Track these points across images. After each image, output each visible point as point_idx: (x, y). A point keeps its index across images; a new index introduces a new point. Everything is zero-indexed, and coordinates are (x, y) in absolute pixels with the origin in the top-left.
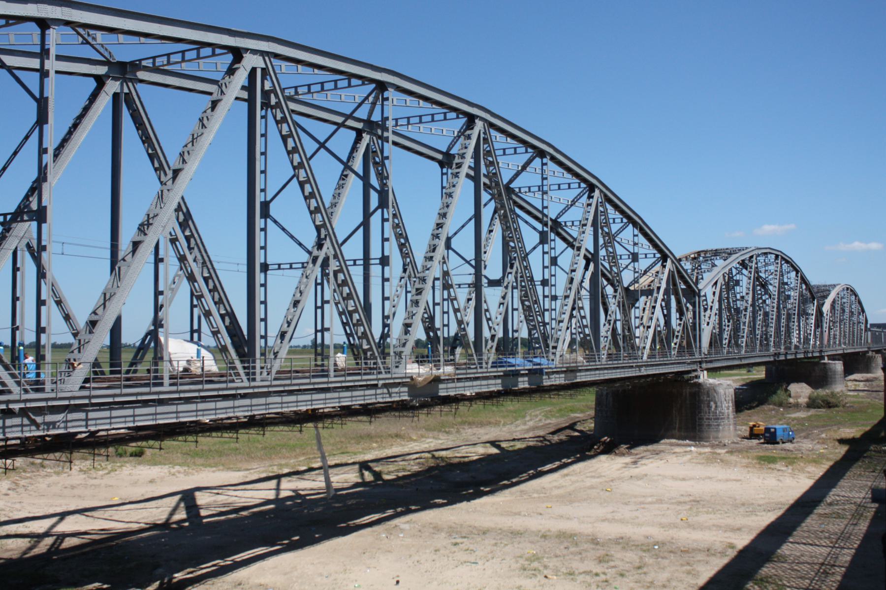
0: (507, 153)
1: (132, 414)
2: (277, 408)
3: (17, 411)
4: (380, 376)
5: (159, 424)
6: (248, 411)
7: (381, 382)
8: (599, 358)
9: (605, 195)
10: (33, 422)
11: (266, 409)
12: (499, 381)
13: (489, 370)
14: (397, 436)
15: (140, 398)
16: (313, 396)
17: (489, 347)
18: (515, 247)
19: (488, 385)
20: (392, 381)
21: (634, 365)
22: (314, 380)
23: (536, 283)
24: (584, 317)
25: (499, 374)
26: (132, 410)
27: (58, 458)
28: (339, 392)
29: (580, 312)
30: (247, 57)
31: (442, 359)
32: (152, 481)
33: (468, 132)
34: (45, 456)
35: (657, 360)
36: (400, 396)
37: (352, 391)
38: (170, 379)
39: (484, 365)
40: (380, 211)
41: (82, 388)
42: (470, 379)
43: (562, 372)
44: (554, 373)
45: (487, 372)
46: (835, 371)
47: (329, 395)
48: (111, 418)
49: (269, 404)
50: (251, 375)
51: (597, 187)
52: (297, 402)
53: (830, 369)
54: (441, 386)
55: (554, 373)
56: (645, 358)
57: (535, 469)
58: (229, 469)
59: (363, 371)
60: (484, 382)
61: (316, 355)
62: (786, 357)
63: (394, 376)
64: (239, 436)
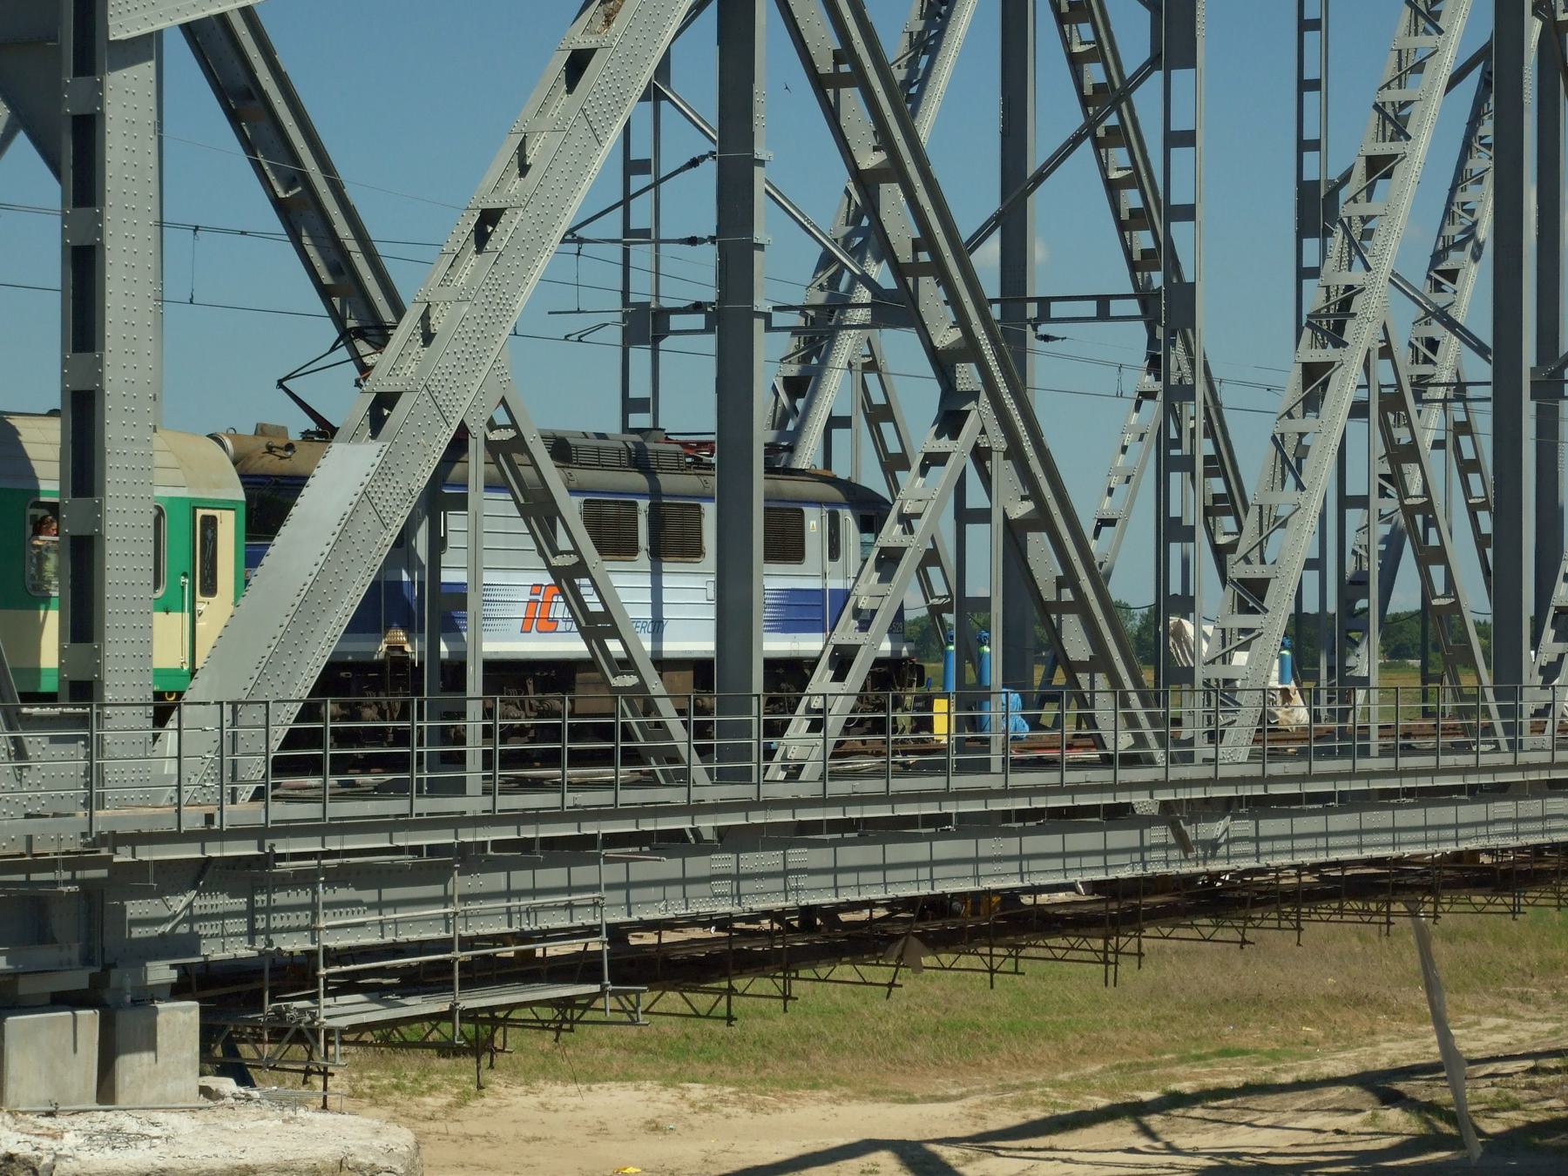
2: (1384, 845)
3: (708, 835)
4: (1363, 764)
5: (1117, 880)
6: (1316, 849)
11: (1394, 845)
14: (1358, 1001)
16: (1400, 814)
19: (785, 873)
20: (883, 811)
23: (1134, 307)
27: (822, 977)
28: (834, 844)
32: (654, 1127)
34: (823, 971)
35: (473, 804)
36: (977, 877)
37: (883, 841)
38: (987, 740)
40: (1157, 77)
42: (1477, 793)
48: (1257, 839)
49: (1493, 823)
52: (1361, 832)
58: (876, 1095)
60: (1471, 812)
61: (1424, 682)
62: (251, 903)
64: (797, 987)
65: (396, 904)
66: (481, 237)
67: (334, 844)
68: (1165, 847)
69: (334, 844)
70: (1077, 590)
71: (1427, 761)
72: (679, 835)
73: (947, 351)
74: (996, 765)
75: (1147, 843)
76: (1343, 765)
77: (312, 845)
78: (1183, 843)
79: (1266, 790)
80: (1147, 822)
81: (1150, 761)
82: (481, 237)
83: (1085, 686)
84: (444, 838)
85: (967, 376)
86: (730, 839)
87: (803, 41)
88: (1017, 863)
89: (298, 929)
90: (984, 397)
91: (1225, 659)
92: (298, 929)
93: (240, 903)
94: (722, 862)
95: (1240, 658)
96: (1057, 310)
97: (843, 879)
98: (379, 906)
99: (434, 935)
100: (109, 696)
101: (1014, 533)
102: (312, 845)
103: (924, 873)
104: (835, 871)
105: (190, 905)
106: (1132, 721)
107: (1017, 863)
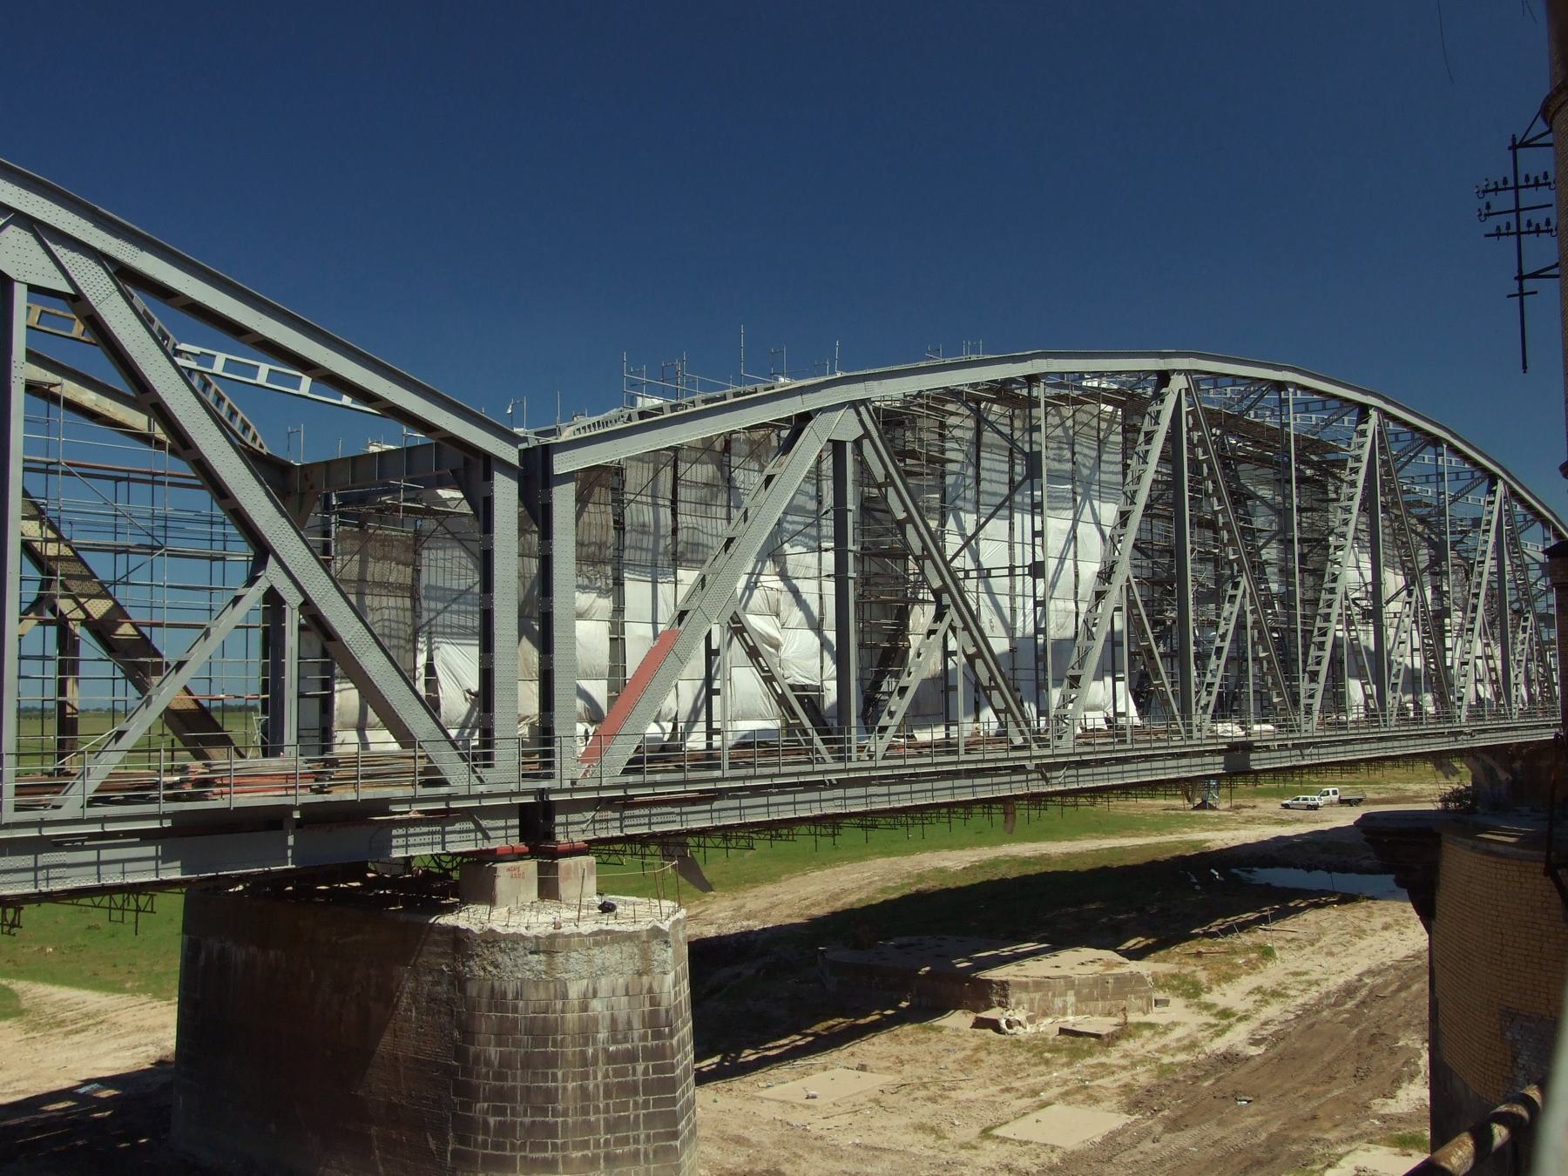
0: (1461, 477)
1: (95, 859)
4: (850, 765)
7: (1447, 730)
8: (1385, 721)
9: (1510, 487)
10: (479, 828)
12: (1220, 759)
13: (1204, 742)
15: (748, 783)
16: (1167, 762)
17: (1203, 703)
18: (1448, 592)
20: (1051, 760)
21: (1290, 743)
22: (936, 760)
24: (1494, 669)
25: (1219, 747)
26: (95, 852)
29: (1487, 663)
30: (1174, 378)
31: (1252, 719)
33: (1362, 427)
39: (1196, 734)
41: (626, 772)
43: (1219, 752)
44: (1309, 745)
45: (1312, 737)
46: (543, 1030)
47: (1127, 767)
50: (841, 755)
51: (1501, 477)
53: (498, 1000)
54: (1253, 756)
55: (1309, 745)
56: (1463, 720)
57: (894, 1006)
59: (1154, 737)
63: (1056, 752)
65: (686, 813)
66: (727, 546)
67: (658, 790)
68: (1038, 780)
69: (658, 790)
70: (996, 682)
71: (928, 760)
72: (823, 782)
73: (938, 589)
74: (1129, 741)
75: (39, 864)
76: (1416, 727)
77: (681, 789)
78: (1303, 756)
79: (103, 828)
80: (1031, 772)
81: (824, 762)
82: (727, 546)
83: (1003, 719)
84: (710, 786)
85: (946, 599)
86: (841, 784)
87: (56, 364)
88: (154, 862)
89: (645, 824)
90: (952, 607)
91: (1065, 706)
92: (645, 824)
93: (617, 815)
94: (839, 792)
95: (1070, 706)
96: (994, 573)
97: (892, 798)
98: (681, 814)
99: (27, 891)
100: (496, 735)
101: (971, 659)
102: (681, 789)
103: (929, 794)
104: (889, 795)
105: (593, 817)
106: (1022, 733)
107: (154, 862)
